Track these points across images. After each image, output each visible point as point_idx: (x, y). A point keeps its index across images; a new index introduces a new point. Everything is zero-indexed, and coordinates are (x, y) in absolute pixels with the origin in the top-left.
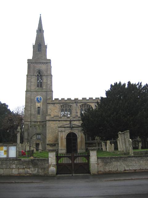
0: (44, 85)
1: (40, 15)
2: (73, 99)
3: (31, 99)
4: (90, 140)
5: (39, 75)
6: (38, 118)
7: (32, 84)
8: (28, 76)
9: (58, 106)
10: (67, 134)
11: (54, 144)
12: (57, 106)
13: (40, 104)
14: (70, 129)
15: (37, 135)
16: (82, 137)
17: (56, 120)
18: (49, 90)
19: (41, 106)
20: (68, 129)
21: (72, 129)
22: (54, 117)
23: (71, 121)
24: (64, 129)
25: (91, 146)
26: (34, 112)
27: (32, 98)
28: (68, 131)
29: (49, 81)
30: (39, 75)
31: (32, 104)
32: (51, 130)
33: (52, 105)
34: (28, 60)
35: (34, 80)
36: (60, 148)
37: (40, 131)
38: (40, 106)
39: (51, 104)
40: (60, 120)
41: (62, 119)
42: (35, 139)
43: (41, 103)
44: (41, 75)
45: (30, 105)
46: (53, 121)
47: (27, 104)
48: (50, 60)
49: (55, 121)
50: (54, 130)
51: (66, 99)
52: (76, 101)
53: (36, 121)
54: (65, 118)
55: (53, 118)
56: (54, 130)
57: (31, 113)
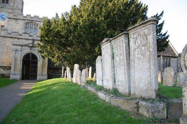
0: (11, 2)
4: (31, 73)
11: (9, 67)
12: (20, 23)
13: (4, 23)
18: (17, 8)
19: (6, 24)
20: (26, 48)
24: (20, 47)
25: (56, 72)
28: (27, 50)
33: (14, 21)
39: (13, 20)
40: (19, 37)
43: (6, 21)
46: (10, 37)
49: (12, 38)
50: (10, 49)
51: (32, 16)
54: (27, 36)
55: (10, 34)
56: (10, 49)
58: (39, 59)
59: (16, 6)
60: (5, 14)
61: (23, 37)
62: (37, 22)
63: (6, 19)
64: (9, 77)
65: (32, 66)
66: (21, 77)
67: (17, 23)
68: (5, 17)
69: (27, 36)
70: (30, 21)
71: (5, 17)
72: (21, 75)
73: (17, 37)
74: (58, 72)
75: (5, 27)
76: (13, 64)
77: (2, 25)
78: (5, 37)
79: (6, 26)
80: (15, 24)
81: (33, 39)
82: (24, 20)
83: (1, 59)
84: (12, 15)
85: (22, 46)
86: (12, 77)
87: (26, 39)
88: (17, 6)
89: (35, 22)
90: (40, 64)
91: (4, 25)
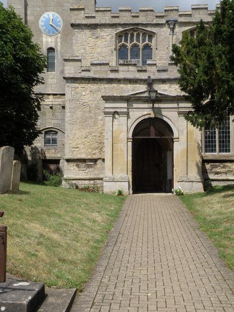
9: (108, 36)
13: (53, 40)
19: (59, 44)
22: (93, 68)
23: (150, 83)
25: (218, 170)
28: (140, 112)
33: (87, 32)
36: (108, 174)
37: (56, 121)
41: (120, 75)
43: (59, 35)
56: (90, 112)
58: (176, 135)
65: (220, 151)
67: (97, 37)
69: (130, 72)
73: (105, 77)
74: (223, 170)
75: (57, 51)
79: (59, 48)
80: (92, 41)
90: (178, 148)
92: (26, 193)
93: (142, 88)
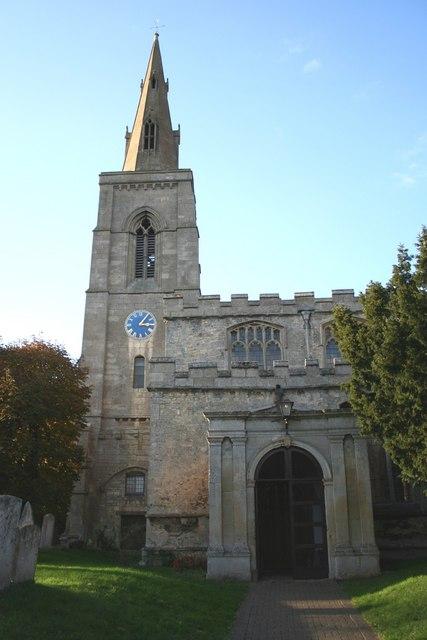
1: (157, 35)
2: (287, 295)
3: (108, 322)
5: (146, 231)
6: (136, 400)
7: (115, 263)
8: (99, 233)
9: (215, 331)
10: (266, 451)
12: (211, 331)
13: (143, 346)
14: (276, 425)
15: (128, 476)
16: (350, 473)
17: (198, 385)
18: (185, 287)
20: (267, 424)
21: (293, 425)
23: (279, 391)
24: (240, 425)
26: (116, 378)
27: (111, 319)
28: (270, 437)
29: (183, 249)
30: (146, 231)
31: (110, 346)
32: (171, 444)
33: (188, 327)
34: (103, 175)
35: (125, 246)
38: (146, 353)
39: (183, 323)
40: (220, 386)
42: (117, 493)
43: (151, 339)
44: (152, 232)
45: (101, 346)
46: (186, 390)
47: (90, 343)
48: (189, 171)
49: (194, 390)
50: (188, 440)
51: (254, 297)
52: (304, 304)
53: (126, 415)
54: (251, 378)
55: (185, 376)
57: (105, 381)
58: (327, 472)
59: (179, 280)
60: (144, 315)
61: (236, 384)
62: (275, 320)
63: (150, 330)
64: (202, 565)
66: (255, 567)
67: (200, 335)
68: (148, 324)
69: (251, 378)
70: (249, 319)
71: (148, 324)
72: (254, 554)
73: (210, 386)
76: (215, 501)
77: (138, 354)
78: (165, 390)
80: (194, 339)
81: (278, 386)
82: (222, 317)
83: (157, 486)
84: (180, 305)
85: (246, 417)
86: (215, 566)
87: (250, 391)
88: (183, 278)
89: (267, 320)
90: (333, 496)
91: (146, 353)
92: (342, 375)
93: (268, 401)
